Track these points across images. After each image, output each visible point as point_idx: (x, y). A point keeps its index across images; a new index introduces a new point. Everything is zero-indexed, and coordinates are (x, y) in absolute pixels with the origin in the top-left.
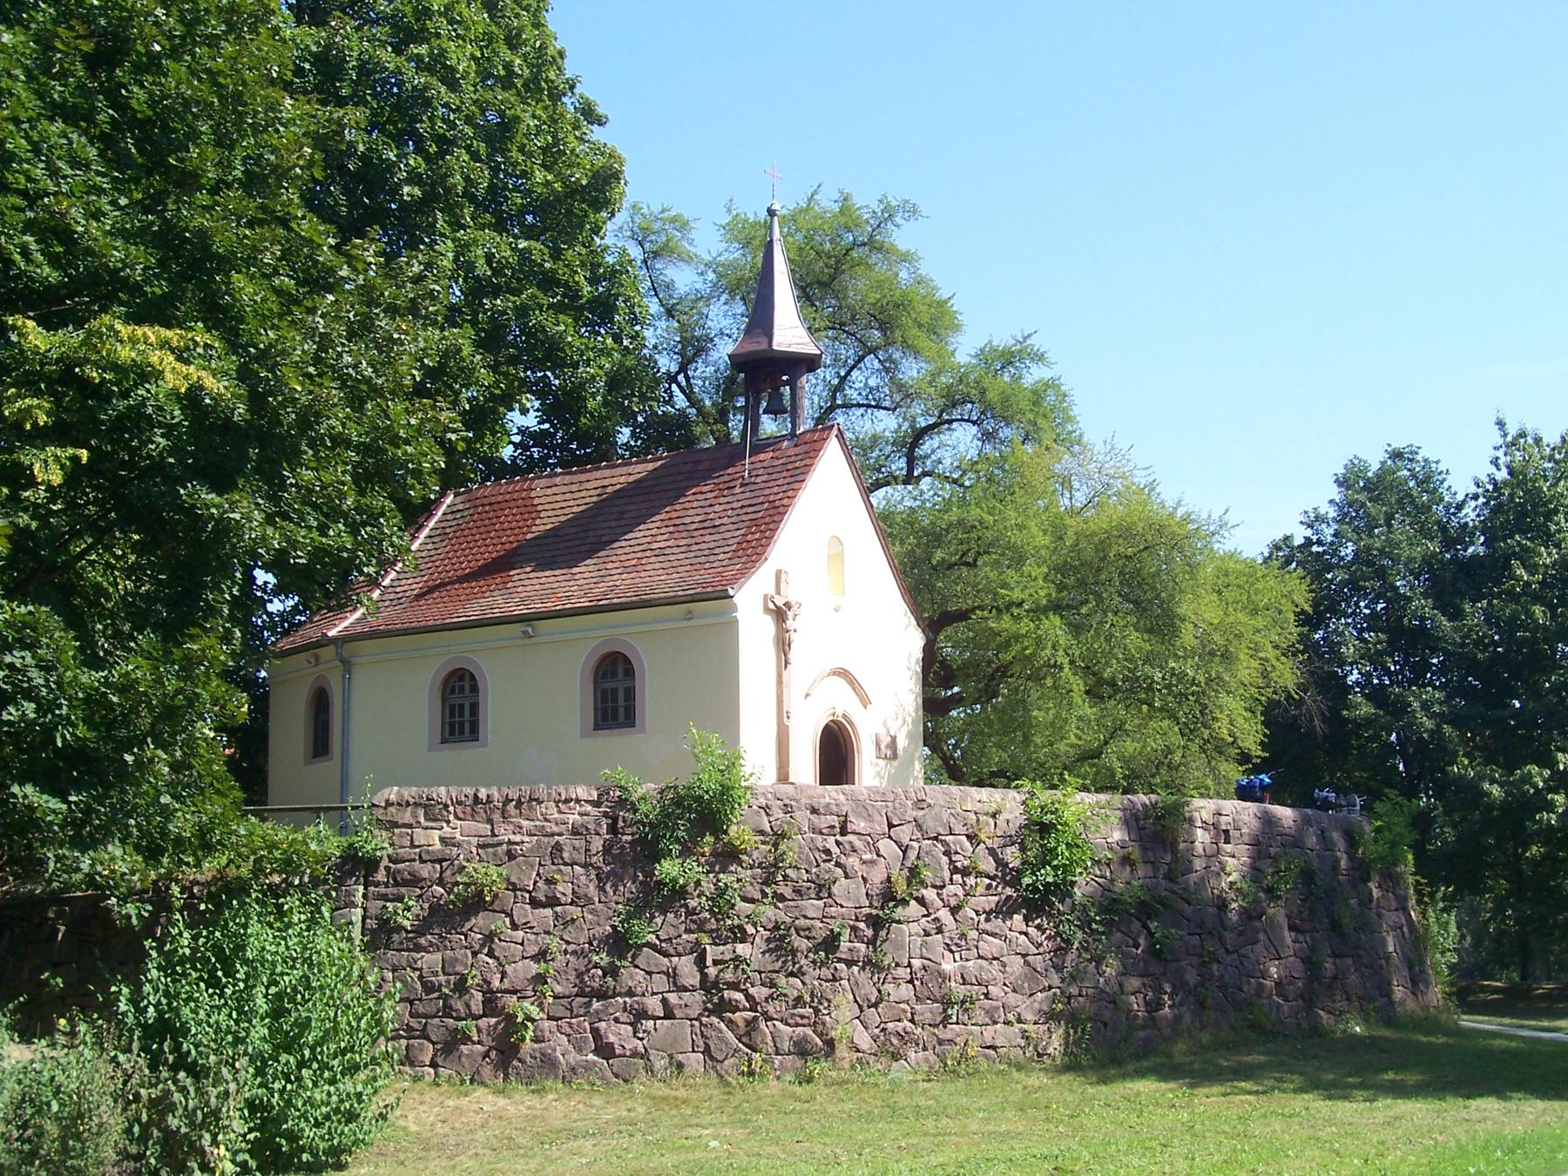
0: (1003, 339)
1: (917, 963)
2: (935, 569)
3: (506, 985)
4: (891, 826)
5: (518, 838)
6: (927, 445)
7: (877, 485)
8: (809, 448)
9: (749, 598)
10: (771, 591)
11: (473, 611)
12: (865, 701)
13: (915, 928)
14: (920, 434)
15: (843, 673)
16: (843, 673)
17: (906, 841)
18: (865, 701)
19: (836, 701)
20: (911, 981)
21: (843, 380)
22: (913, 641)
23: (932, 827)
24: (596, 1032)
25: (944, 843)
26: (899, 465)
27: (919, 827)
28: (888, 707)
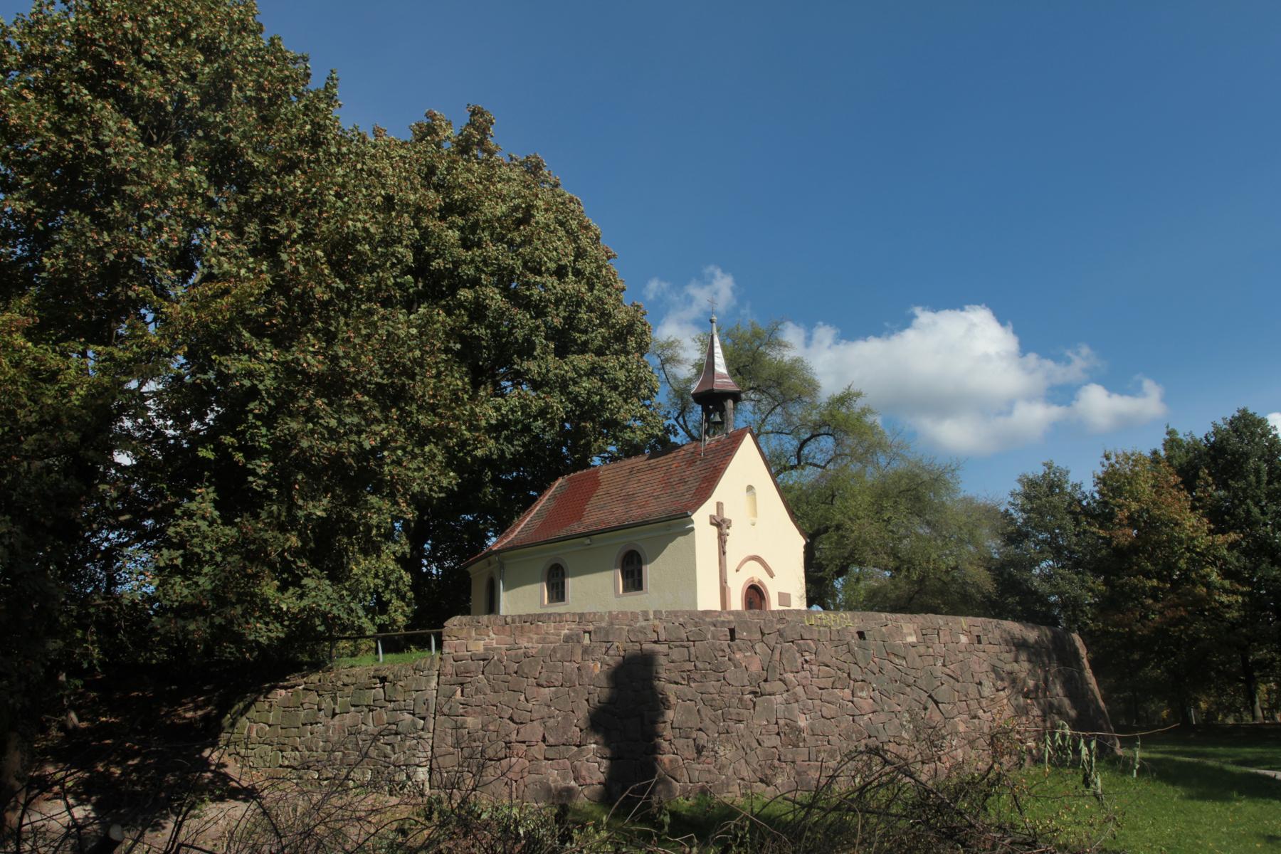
0: (838, 391)
1: (781, 722)
2: (812, 513)
3: (519, 738)
4: (763, 634)
5: (530, 645)
6: (806, 451)
7: (779, 472)
8: (736, 440)
9: (701, 518)
10: (715, 513)
11: (562, 533)
12: (772, 575)
13: (779, 698)
14: (803, 444)
15: (756, 558)
16: (756, 558)
17: (773, 644)
18: (772, 575)
19: (755, 572)
20: (778, 734)
21: (763, 421)
22: (798, 543)
23: (791, 634)
24: (574, 769)
25: (798, 645)
26: (794, 461)
27: (781, 635)
28: (788, 584)
